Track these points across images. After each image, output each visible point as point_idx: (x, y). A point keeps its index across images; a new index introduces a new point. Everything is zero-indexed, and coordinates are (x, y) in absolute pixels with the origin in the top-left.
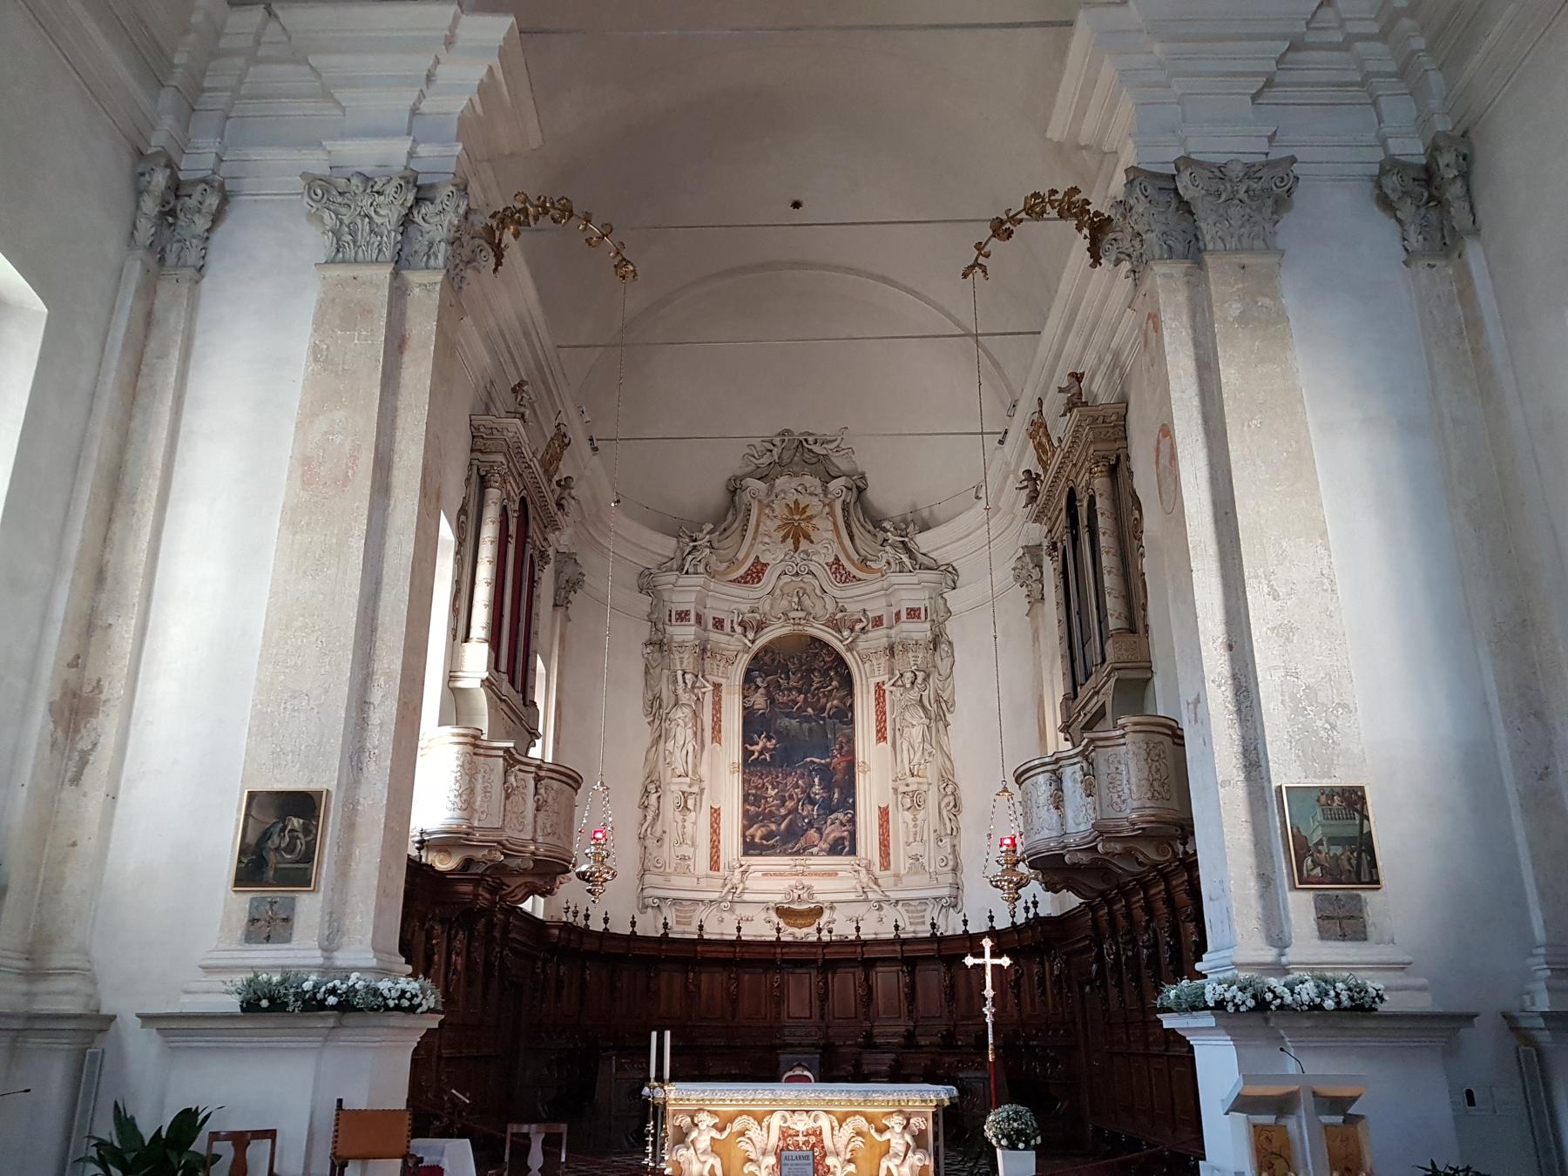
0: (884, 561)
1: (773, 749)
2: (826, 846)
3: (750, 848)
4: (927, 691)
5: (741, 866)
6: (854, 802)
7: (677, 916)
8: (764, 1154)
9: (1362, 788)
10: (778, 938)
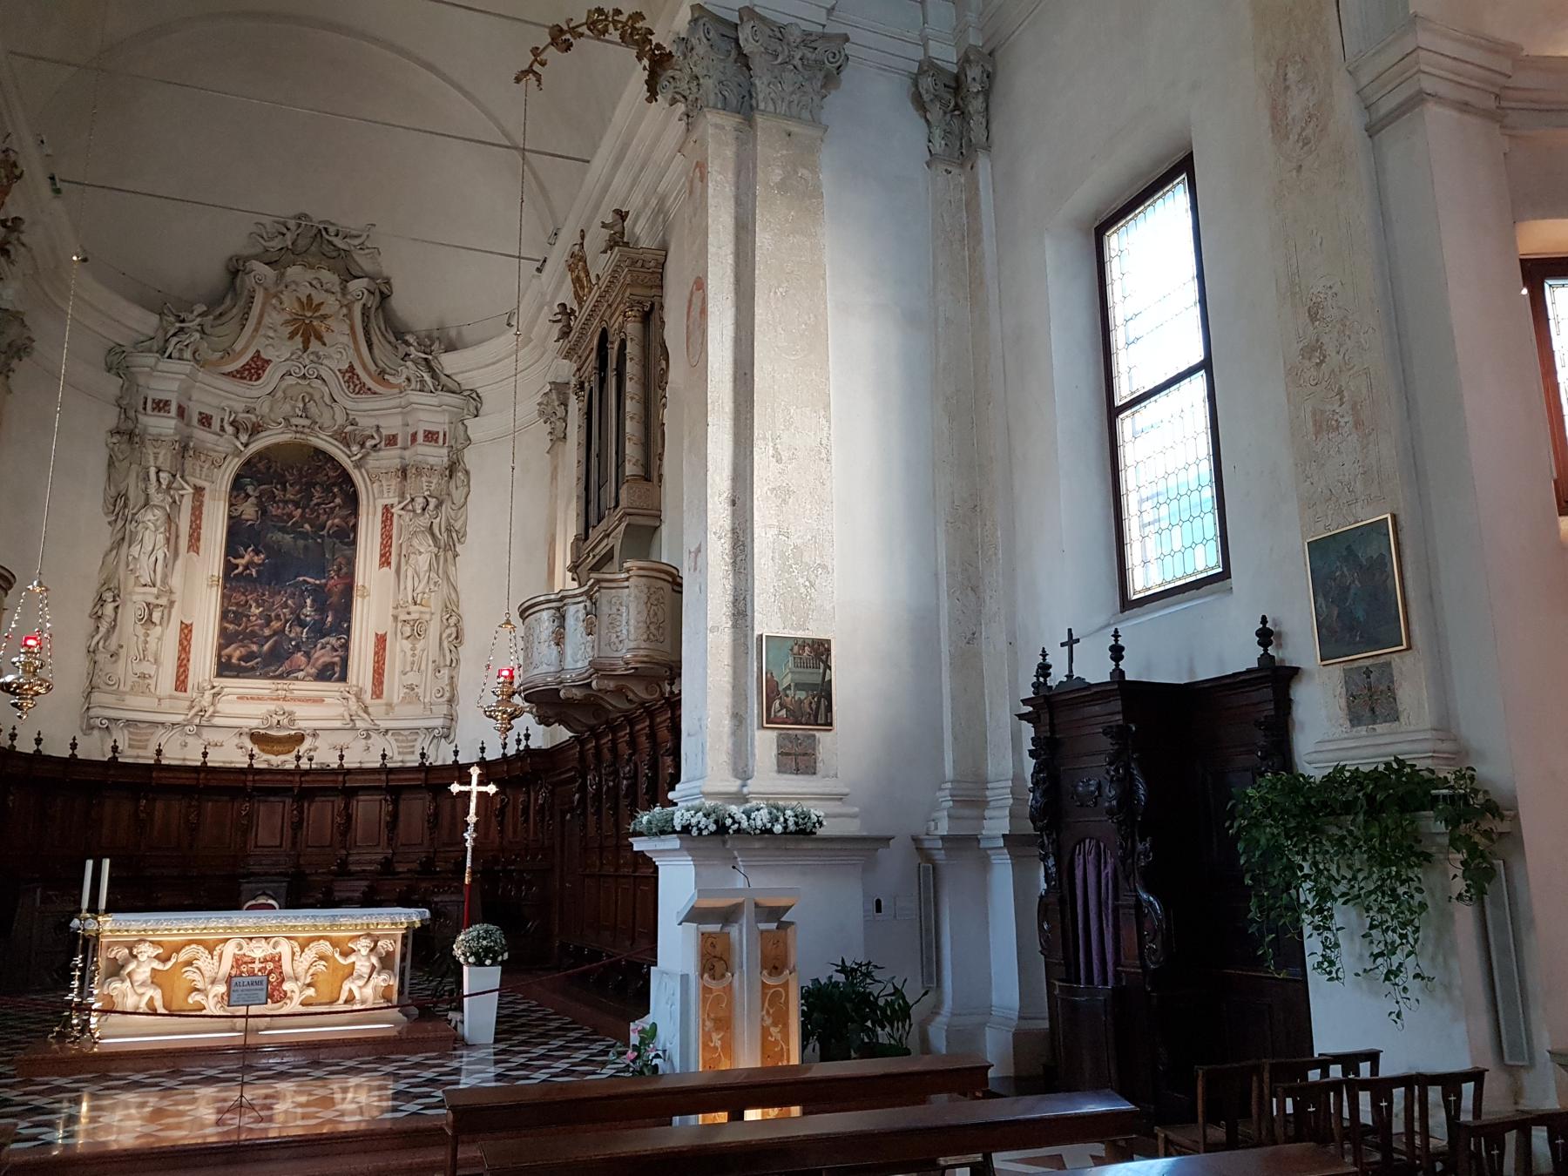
0: (404, 376)
1: (259, 565)
2: (313, 671)
3: (225, 668)
4: (438, 519)
5: (213, 687)
6: (349, 627)
7: (130, 739)
8: (213, 982)
9: (829, 642)
10: (251, 765)
